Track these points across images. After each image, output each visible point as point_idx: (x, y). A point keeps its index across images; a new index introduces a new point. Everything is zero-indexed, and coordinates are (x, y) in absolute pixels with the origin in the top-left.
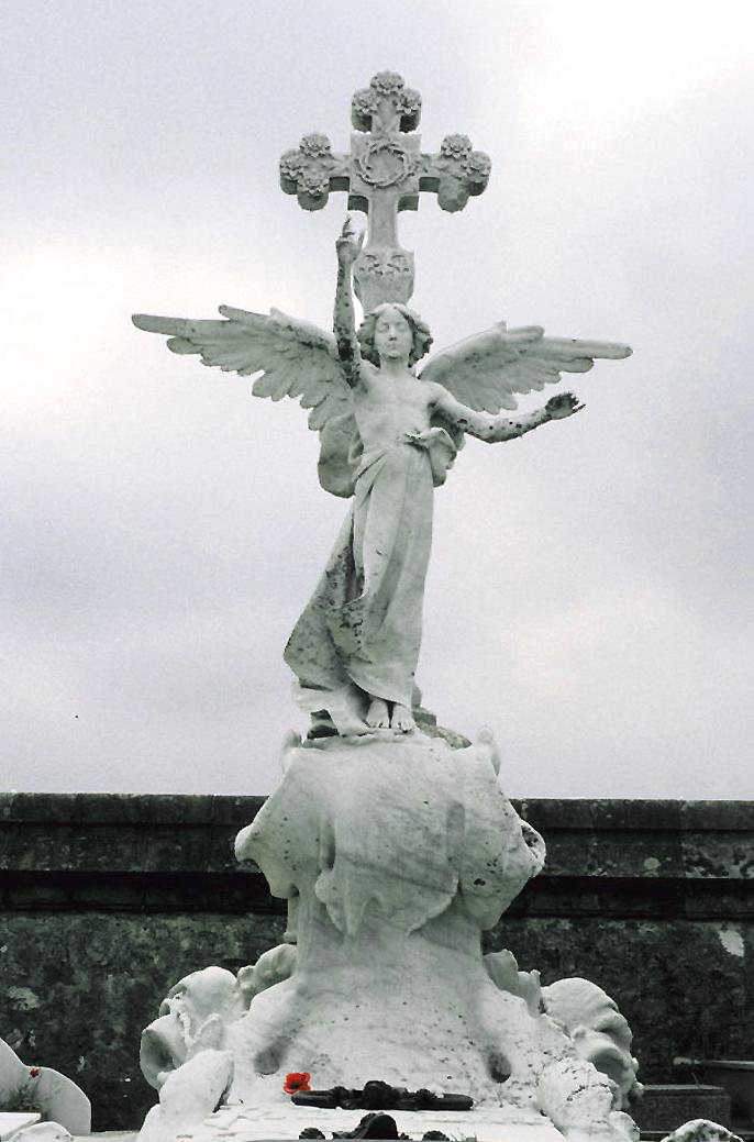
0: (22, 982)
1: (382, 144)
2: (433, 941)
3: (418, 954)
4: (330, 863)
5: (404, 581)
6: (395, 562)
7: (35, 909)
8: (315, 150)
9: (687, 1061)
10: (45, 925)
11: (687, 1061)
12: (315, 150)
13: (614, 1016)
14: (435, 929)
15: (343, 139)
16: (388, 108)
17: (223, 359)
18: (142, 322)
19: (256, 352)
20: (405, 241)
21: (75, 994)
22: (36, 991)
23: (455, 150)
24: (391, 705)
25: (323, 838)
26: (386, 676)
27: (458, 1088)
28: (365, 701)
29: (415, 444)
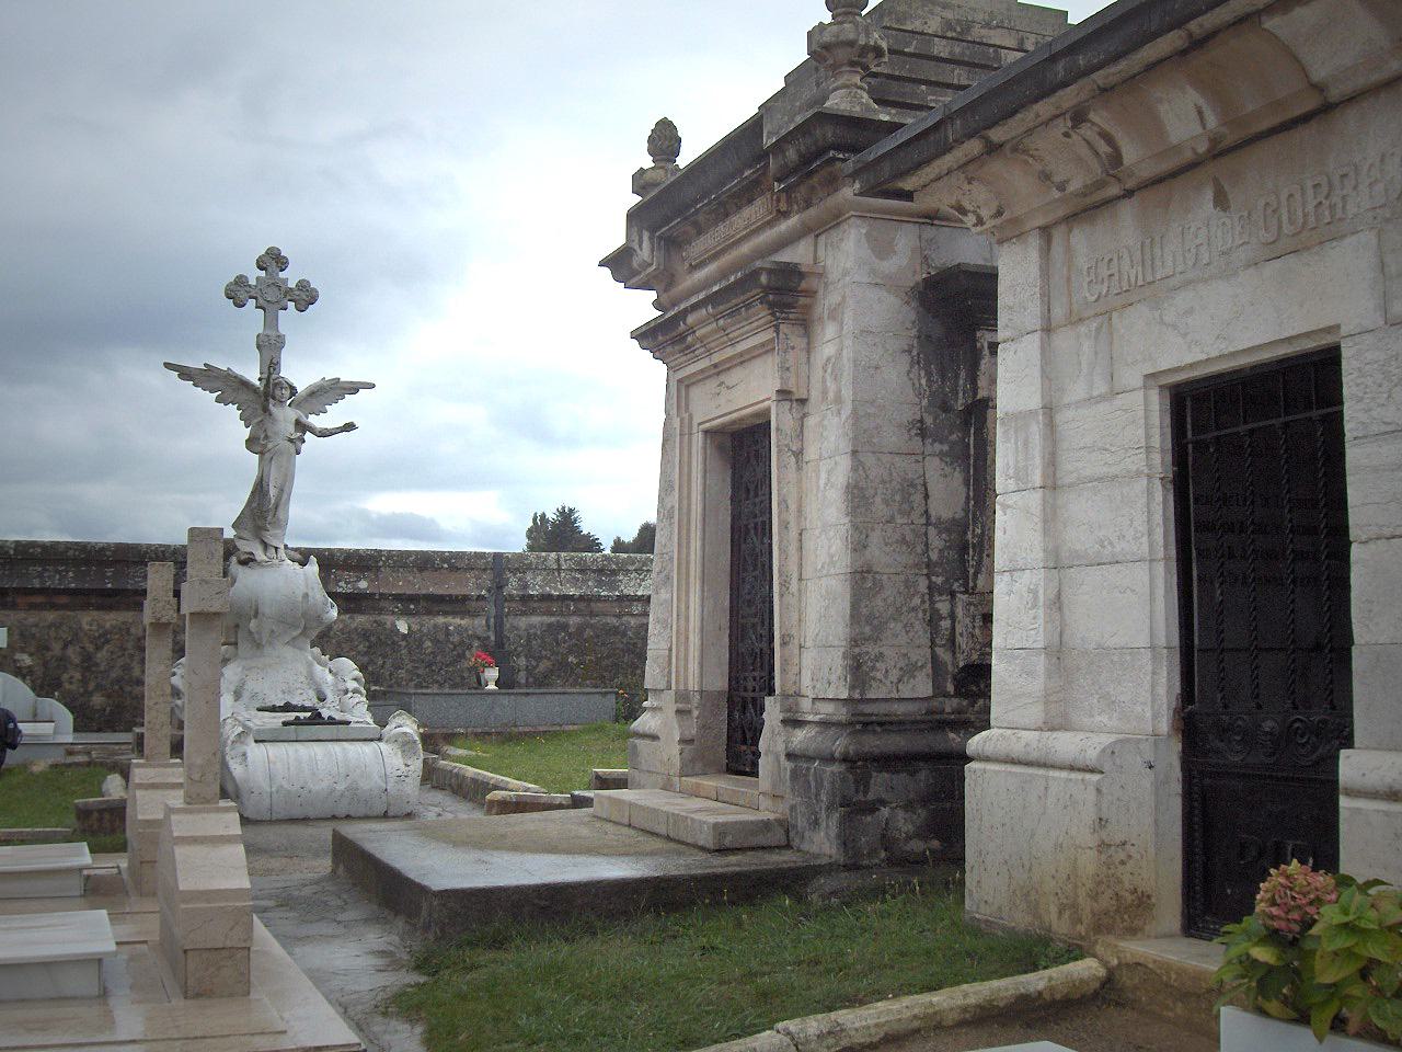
0: (23, 650)
1: (271, 281)
2: (294, 647)
3: (289, 652)
4: (256, 616)
5: (285, 496)
6: (279, 498)
7: (32, 607)
8: (241, 281)
9: (377, 688)
10: (32, 618)
11: (377, 688)
12: (241, 281)
13: (358, 673)
14: (293, 642)
15: (254, 275)
16: (273, 260)
17: (205, 385)
18: (167, 365)
19: (217, 384)
20: (282, 330)
21: (52, 657)
22: (31, 655)
23: (303, 285)
24: (276, 548)
25: (254, 607)
26: (275, 536)
27: (971, 872)
28: (266, 546)
29: (291, 440)
